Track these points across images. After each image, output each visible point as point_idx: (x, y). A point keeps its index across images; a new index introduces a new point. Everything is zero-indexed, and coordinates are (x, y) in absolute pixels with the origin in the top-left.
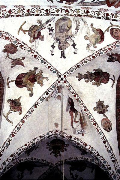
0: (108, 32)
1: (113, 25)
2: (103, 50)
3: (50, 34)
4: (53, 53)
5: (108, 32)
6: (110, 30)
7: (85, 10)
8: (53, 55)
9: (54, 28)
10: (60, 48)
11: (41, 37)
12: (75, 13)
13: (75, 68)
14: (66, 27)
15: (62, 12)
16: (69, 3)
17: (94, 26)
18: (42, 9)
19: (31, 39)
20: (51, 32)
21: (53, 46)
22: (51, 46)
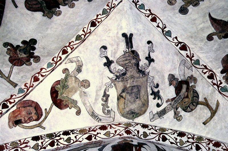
0: (46, 109)
1: (39, 126)
2: (47, 73)
3: (157, 86)
4: (148, 45)
5: (46, 109)
6: (42, 115)
7: (95, 140)
8: (149, 42)
9: (151, 97)
10: (135, 54)
11: (175, 82)
12: (112, 131)
13: (99, 20)
14: (128, 97)
15: (136, 132)
16: (127, 142)
17: (74, 110)
18: (173, 143)
19: (193, 84)
20: (156, 90)
21: (150, 60)
22: (153, 60)
